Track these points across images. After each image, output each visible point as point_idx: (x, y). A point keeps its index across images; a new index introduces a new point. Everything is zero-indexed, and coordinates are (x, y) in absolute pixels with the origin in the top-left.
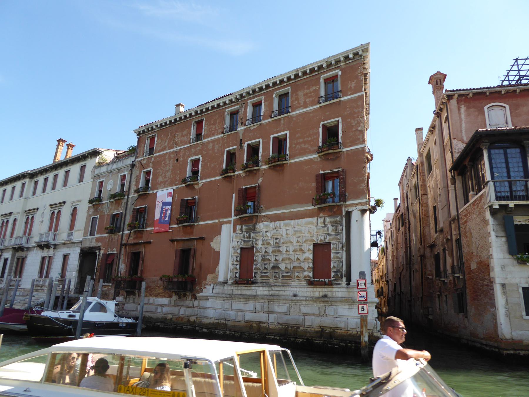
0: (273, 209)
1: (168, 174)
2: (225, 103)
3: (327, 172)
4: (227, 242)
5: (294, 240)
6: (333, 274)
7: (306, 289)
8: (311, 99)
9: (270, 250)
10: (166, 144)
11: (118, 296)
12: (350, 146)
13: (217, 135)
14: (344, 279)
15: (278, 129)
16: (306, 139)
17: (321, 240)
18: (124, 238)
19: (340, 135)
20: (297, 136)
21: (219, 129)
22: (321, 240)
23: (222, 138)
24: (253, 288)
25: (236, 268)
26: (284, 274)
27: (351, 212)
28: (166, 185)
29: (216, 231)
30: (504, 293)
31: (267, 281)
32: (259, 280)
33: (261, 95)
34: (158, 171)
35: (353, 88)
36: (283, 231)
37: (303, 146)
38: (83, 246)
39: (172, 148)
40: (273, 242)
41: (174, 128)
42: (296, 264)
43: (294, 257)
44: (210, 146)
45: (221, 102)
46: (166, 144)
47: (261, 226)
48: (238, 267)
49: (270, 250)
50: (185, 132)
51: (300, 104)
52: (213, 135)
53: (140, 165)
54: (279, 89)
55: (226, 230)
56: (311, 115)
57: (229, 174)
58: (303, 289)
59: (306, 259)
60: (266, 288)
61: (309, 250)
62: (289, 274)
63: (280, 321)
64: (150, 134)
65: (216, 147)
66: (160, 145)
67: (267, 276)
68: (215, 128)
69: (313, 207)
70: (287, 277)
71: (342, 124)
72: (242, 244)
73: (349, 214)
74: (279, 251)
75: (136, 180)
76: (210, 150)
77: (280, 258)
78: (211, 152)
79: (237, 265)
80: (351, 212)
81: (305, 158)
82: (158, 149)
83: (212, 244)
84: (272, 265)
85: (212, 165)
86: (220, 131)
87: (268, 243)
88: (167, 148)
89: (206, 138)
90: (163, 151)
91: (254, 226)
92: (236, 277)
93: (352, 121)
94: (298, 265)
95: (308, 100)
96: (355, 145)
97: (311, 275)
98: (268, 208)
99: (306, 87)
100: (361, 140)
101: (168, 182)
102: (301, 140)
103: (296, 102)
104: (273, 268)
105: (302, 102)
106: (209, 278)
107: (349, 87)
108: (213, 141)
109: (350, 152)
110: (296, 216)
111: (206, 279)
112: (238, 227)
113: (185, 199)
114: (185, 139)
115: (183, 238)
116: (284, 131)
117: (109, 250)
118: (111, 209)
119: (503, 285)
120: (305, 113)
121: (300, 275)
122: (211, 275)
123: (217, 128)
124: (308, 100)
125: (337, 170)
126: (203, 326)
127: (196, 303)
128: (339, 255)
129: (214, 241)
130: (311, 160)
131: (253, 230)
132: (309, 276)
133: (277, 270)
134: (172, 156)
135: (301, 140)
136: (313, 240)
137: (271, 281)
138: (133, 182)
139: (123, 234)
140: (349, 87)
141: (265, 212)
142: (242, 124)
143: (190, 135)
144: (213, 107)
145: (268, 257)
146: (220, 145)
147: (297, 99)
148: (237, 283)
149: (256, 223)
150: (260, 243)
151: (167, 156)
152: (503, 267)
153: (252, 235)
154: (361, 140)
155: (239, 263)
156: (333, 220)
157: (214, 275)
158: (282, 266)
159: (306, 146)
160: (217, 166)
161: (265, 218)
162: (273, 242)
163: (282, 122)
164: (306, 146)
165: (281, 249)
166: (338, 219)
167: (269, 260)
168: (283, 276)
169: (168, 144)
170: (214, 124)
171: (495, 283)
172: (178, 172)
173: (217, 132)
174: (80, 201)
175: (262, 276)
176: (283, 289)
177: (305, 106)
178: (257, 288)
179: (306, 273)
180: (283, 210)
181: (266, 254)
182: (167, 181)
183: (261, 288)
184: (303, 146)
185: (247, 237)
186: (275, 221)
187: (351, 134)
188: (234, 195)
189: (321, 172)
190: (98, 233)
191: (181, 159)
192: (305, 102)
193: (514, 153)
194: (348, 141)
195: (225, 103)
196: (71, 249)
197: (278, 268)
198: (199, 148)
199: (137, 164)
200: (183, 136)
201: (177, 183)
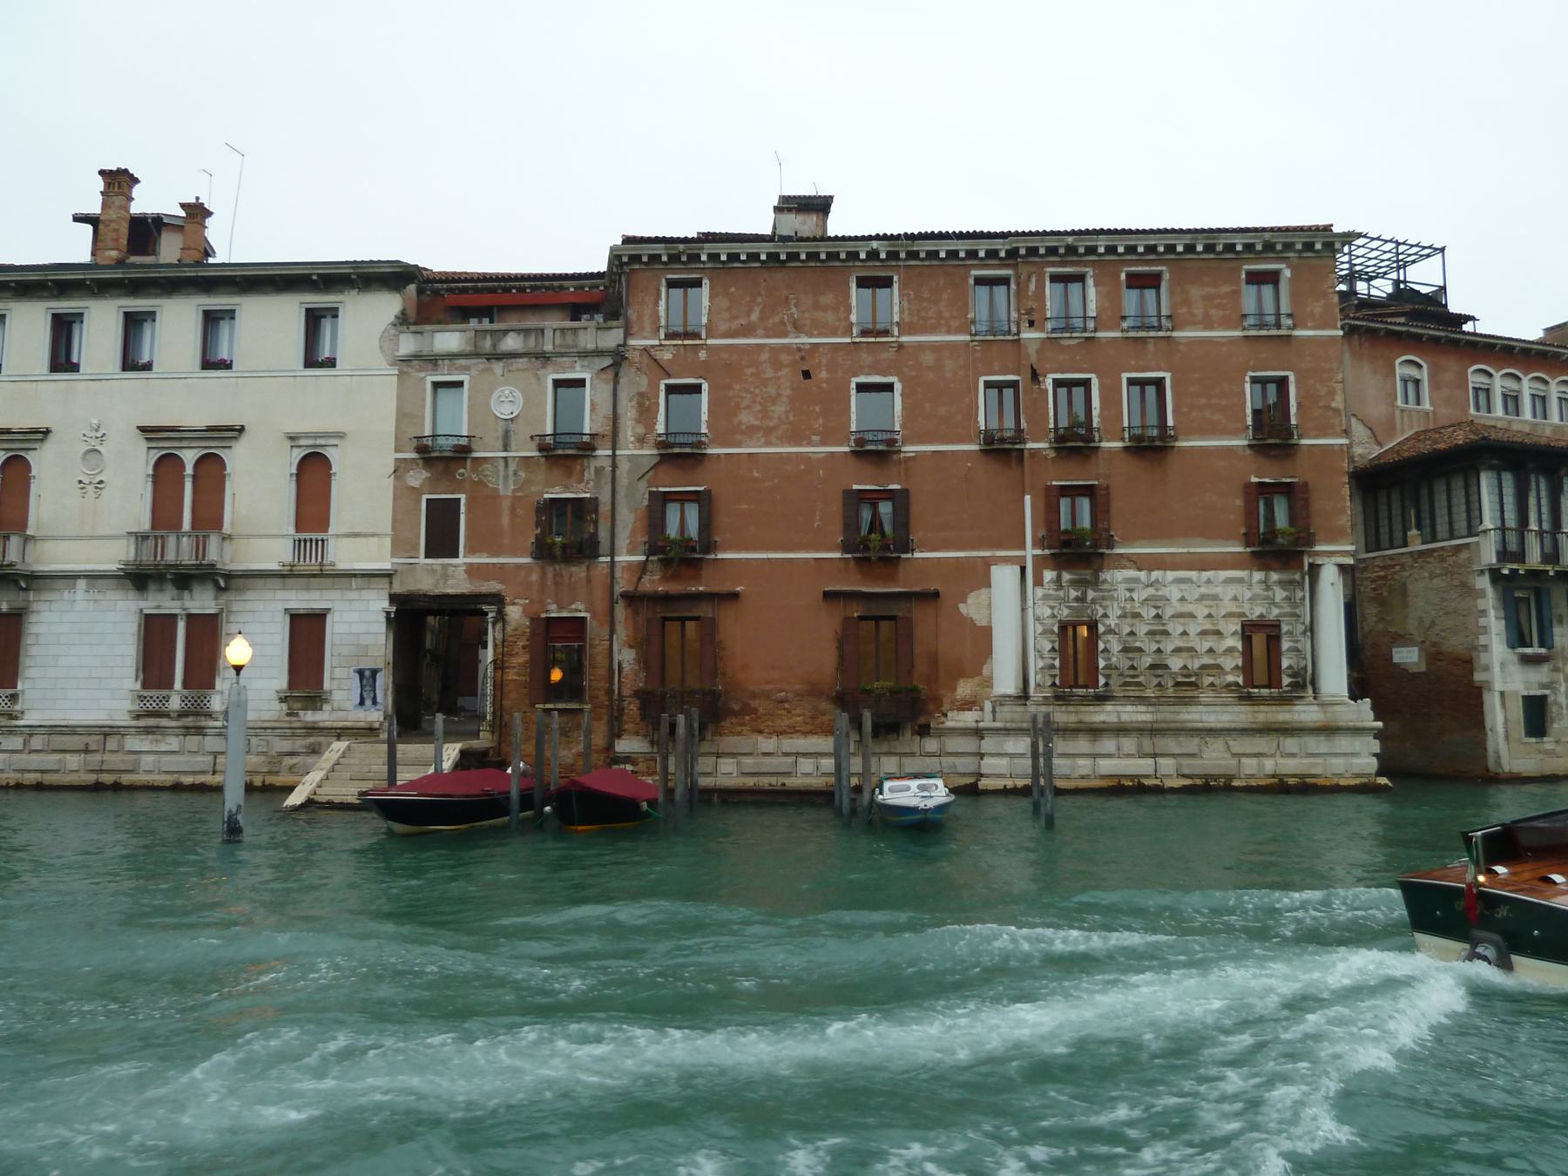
1: (779, 410)
2: (972, 254)
5: (1201, 611)
6: (1286, 681)
7: (1237, 709)
8: (1221, 313)
9: (1142, 629)
10: (755, 317)
11: (619, 737)
12: (1315, 437)
13: (949, 332)
14: (1310, 690)
15: (1142, 363)
16: (1214, 401)
18: (618, 574)
23: (966, 344)
25: (1053, 667)
26: (1180, 679)
27: (1319, 566)
28: (774, 440)
29: (979, 577)
30: (1503, 705)
34: (731, 394)
36: (1174, 593)
37: (1207, 414)
38: (398, 588)
39: (784, 335)
41: (779, 277)
42: (1207, 660)
46: (755, 317)
47: (1116, 577)
48: (1057, 663)
50: (828, 299)
51: (1194, 315)
52: (934, 330)
53: (646, 360)
54: (1136, 263)
55: (1004, 578)
58: (1230, 709)
59: (1230, 650)
60: (1143, 708)
63: (1186, 771)
65: (949, 365)
66: (727, 315)
67: (1139, 684)
68: (940, 316)
69: (1241, 549)
70: (1187, 687)
71: (1298, 388)
73: (1315, 570)
74: (1166, 633)
75: (640, 404)
76: (929, 368)
77: (1168, 646)
80: (1319, 566)
82: (723, 327)
83: (963, 608)
84: (1147, 661)
85: (942, 411)
86: (955, 323)
87: (1137, 615)
88: (760, 332)
89: (910, 334)
90: (744, 336)
91: (1097, 577)
93: (1318, 386)
95: (1213, 312)
97: (1240, 680)
98: (1128, 540)
99: (1206, 279)
101: (780, 433)
102: (1203, 401)
104: (1153, 667)
105: (1199, 311)
106: (964, 689)
108: (935, 347)
110: (1202, 563)
112: (1049, 575)
113: (855, 487)
114: (830, 317)
115: (865, 589)
116: (1159, 370)
118: (527, 481)
119: (1502, 694)
120: (1209, 340)
121: (1217, 682)
123: (946, 314)
124: (1213, 312)
127: (931, 744)
128: (1299, 646)
130: (1229, 449)
131: (1095, 583)
132: (1237, 684)
133: (1159, 672)
134: (784, 357)
135: (1203, 401)
136: (1243, 615)
137: (1149, 693)
138: (628, 413)
139: (613, 562)
142: (1031, 323)
143: (849, 311)
145: (1138, 644)
146: (961, 362)
147: (1187, 302)
148: (1060, 698)
149: (1100, 569)
150: (1114, 612)
151: (765, 356)
152: (1503, 665)
153: (1091, 594)
155: (1057, 655)
156: (1285, 576)
157: (977, 680)
158: (1175, 664)
159: (1217, 417)
160: (959, 417)
163: (1151, 347)
164: (1217, 417)
165: (1169, 628)
166: (1297, 577)
167: (1140, 650)
168: (1178, 684)
169: (761, 319)
171: (1490, 690)
172: (817, 409)
174: (341, 435)
177: (1209, 326)
178: (1119, 708)
179: (1230, 678)
182: (775, 428)
183: (1129, 708)
184: (1207, 414)
185: (1077, 599)
186: (1151, 570)
188: (1028, 498)
189: (1254, 480)
191: (824, 375)
192: (1206, 316)
193: (1539, 490)
195: (972, 254)
196: (335, 594)
197: (1166, 667)
198: (884, 355)
199: (633, 356)
200: (817, 306)
201: (814, 438)
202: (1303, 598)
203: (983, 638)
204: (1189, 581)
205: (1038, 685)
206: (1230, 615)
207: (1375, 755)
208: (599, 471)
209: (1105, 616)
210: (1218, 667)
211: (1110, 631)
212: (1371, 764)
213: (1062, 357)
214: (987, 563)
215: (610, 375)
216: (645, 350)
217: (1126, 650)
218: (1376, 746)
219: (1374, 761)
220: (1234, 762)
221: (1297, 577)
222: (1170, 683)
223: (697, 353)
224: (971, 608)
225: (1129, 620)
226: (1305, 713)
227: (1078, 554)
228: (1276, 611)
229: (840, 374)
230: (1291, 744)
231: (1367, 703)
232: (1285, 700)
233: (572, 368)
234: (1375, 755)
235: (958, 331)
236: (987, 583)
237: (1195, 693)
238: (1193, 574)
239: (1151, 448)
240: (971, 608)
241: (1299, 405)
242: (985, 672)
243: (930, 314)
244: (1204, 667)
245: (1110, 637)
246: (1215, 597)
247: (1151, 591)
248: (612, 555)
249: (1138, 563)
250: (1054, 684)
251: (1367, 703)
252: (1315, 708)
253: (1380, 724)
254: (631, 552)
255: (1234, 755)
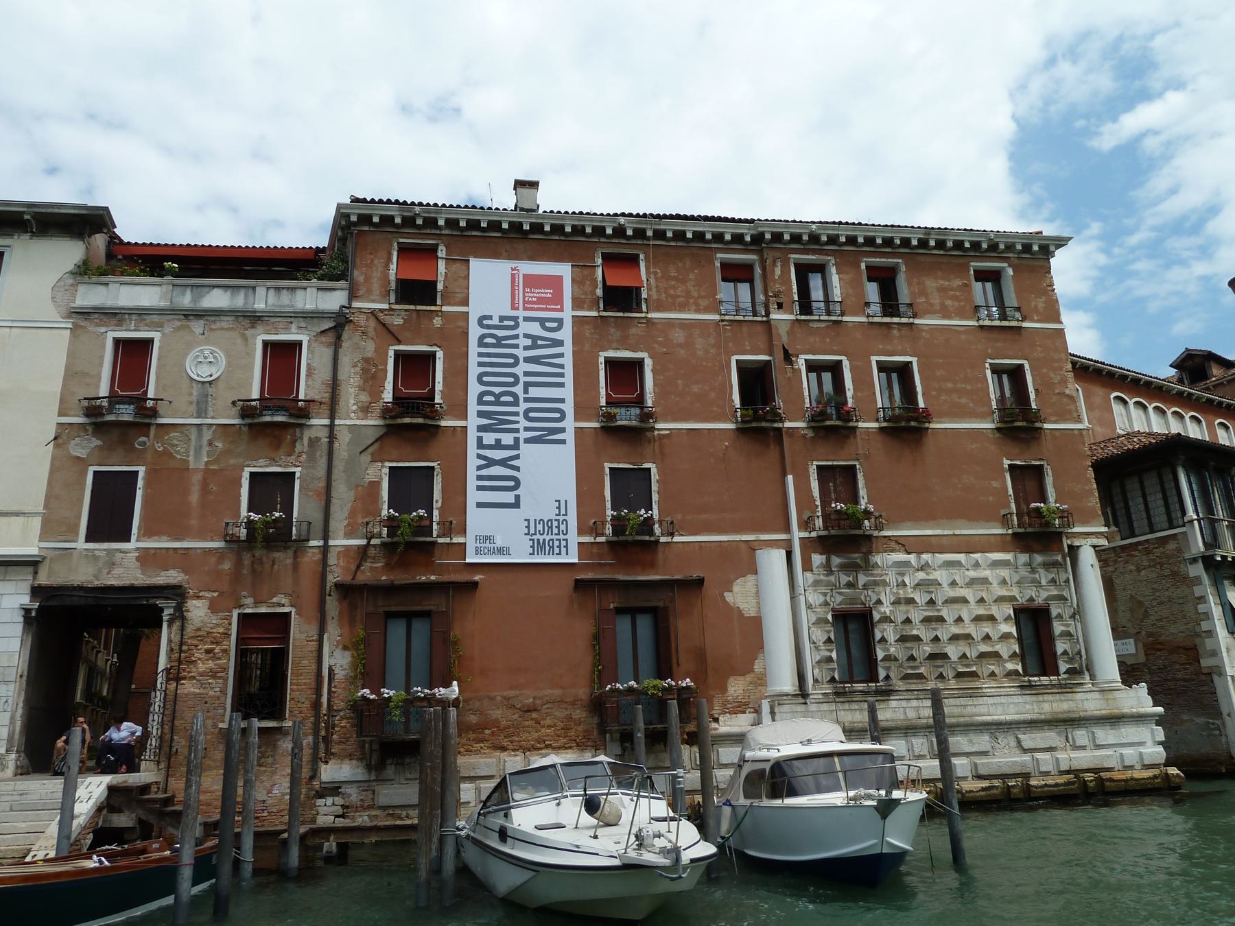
0: (909, 524)
3: (1018, 463)
4: (780, 597)
6: (1063, 667)
8: (957, 304)
13: (698, 311)
15: (889, 347)
16: (959, 386)
17: (1031, 599)
18: (332, 560)
19: (1032, 396)
20: (938, 374)
21: (700, 297)
22: (1031, 599)
24: (894, 704)
25: (830, 659)
27: (1078, 547)
31: (920, 687)
32: (900, 685)
33: (827, 253)
35: (1041, 310)
36: (941, 576)
38: (43, 579)
40: (920, 598)
42: (984, 648)
43: (976, 631)
44: (678, 336)
45: (709, 230)
47: (885, 559)
48: (834, 655)
49: (916, 616)
51: (932, 305)
52: (683, 308)
53: (372, 323)
55: (773, 562)
56: (963, 337)
57: (764, 424)
59: (1005, 637)
61: (1007, 619)
62: (974, 669)
63: (983, 772)
64: (408, 235)
68: (688, 293)
72: (837, 600)
74: (941, 620)
76: (680, 345)
78: (682, 351)
79: (831, 651)
81: (966, 423)
83: (728, 596)
85: (695, 389)
87: (911, 601)
89: (658, 310)
92: (833, 680)
93: (1052, 375)
94: (990, 649)
96: (1065, 421)
100: (1075, 415)
103: (923, 300)
104: (932, 657)
106: (736, 688)
107: (1033, 304)
109: (1057, 433)
110: (969, 546)
111: (724, 689)
112: (818, 559)
117: (250, 601)
122: (741, 678)
123: (695, 294)
125: (1038, 463)
126: (977, 810)
129: (736, 588)
132: (1016, 672)
133: (939, 662)
135: (950, 385)
136: (1013, 599)
140: (1033, 304)
141: (889, 529)
142: (780, 306)
144: (699, 236)
145: (915, 632)
147: (923, 292)
150: (887, 597)
154: (1075, 415)
155: (833, 646)
157: (749, 677)
158: (953, 651)
159: (964, 401)
161: (893, 544)
162: (920, 598)
164: (964, 401)
165: (944, 613)
167: (917, 639)
168: (959, 675)
170: (684, 282)
173: (697, 305)
175: (906, 677)
176: (970, 701)
178: (904, 703)
179: (1010, 666)
180: (989, 528)
181: (907, 627)
184: (955, 397)
186: (919, 553)
187: (1054, 399)
190: (147, 532)
194: (1050, 411)
202: (1067, 581)
203: (753, 631)
204: (958, 564)
205: (816, 681)
206: (1000, 600)
207: (1160, 743)
208: (313, 442)
209: (879, 602)
210: (996, 655)
211: (886, 619)
212: (1156, 753)
213: (811, 339)
214: (752, 548)
215: (330, 338)
216: (373, 313)
217: (903, 639)
218: (1160, 734)
219: (1161, 749)
220: (1027, 758)
221: (1059, 558)
222: (951, 674)
223: (431, 319)
224: (740, 595)
225: (903, 608)
226: (1088, 702)
227: (845, 541)
228: (1044, 594)
229: (587, 347)
230: (1081, 736)
231: (1142, 689)
232: (1065, 688)
233: (287, 330)
234: (1160, 743)
235: (707, 310)
236: (752, 568)
237: (977, 684)
238: (961, 557)
239: (907, 427)
240: (740, 595)
241: (1036, 390)
242: (758, 667)
243: (678, 293)
244: (982, 655)
245: (885, 626)
246: (985, 581)
247: (921, 575)
248: (326, 538)
249: (903, 544)
250: (833, 680)
251: (1142, 689)
252: (1097, 695)
253: (1160, 710)
254: (348, 535)
255: (1025, 751)
